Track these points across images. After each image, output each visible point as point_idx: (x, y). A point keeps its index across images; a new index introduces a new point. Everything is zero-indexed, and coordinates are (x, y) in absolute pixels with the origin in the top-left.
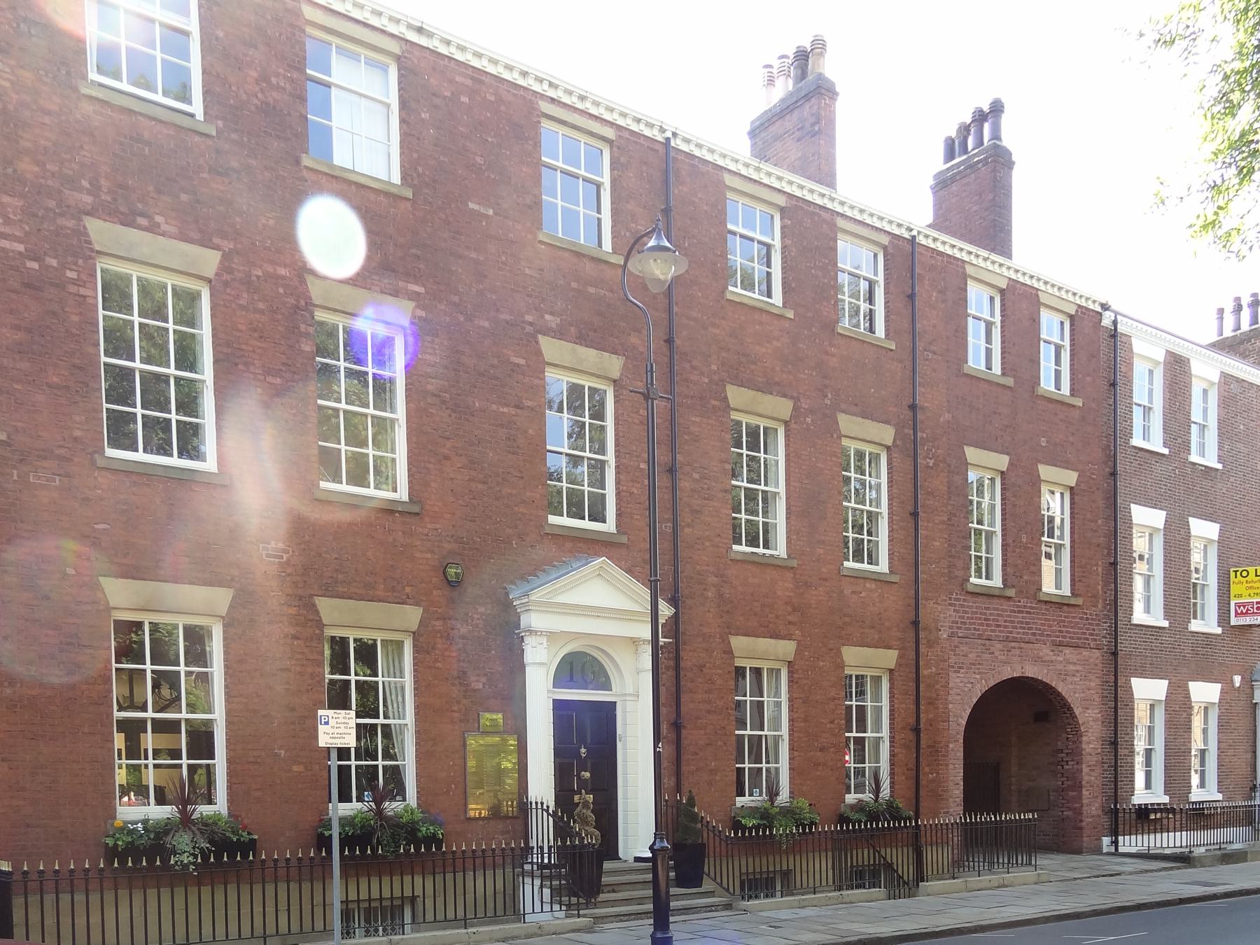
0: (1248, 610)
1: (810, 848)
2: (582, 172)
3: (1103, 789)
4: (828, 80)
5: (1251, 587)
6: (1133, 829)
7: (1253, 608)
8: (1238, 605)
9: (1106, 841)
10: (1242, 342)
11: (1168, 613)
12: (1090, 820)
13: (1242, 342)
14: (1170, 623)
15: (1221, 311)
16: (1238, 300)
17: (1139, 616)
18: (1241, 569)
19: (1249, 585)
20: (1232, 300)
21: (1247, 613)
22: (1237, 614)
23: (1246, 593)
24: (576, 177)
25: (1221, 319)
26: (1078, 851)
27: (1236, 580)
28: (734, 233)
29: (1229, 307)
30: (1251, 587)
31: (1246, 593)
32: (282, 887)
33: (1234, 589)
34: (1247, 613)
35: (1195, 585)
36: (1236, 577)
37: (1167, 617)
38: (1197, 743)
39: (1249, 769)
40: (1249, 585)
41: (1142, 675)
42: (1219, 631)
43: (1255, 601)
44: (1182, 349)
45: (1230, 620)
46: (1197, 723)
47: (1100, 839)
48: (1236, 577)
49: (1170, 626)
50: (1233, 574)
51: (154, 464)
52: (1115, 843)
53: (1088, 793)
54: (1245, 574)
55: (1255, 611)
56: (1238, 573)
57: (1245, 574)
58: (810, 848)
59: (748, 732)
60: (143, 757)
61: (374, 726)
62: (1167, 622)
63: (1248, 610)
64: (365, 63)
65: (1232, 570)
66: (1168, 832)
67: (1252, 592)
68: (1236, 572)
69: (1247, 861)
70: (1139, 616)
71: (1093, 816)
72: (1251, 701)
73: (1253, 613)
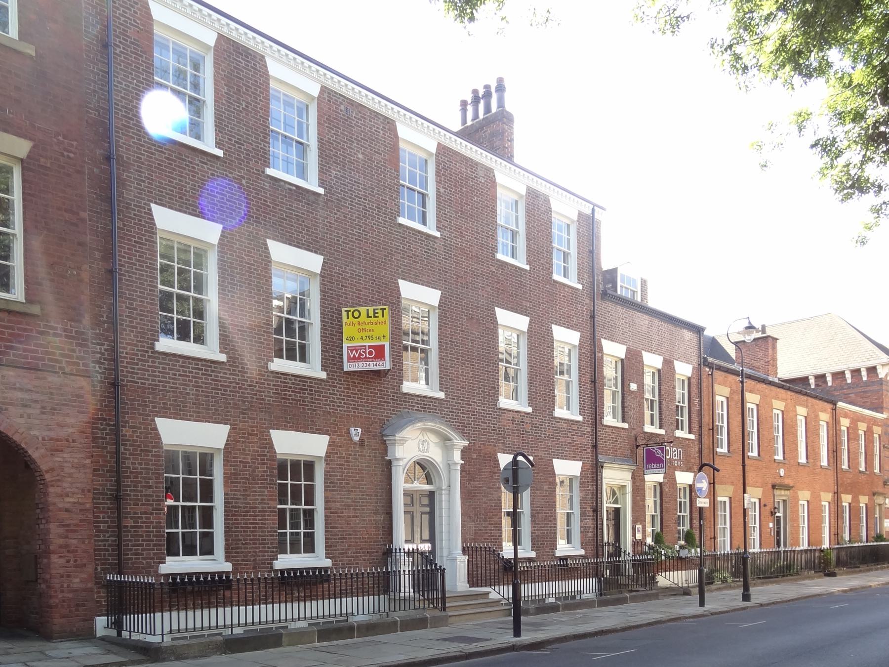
0: (360, 354)
1: (530, 581)
2: (418, 188)
3: (96, 555)
4: (507, 112)
5: (363, 330)
6: (276, 597)
7: (365, 352)
8: (351, 349)
9: (101, 623)
10: (477, 131)
11: (532, 400)
12: (70, 595)
13: (477, 131)
14: (327, 374)
15: (464, 104)
16: (475, 92)
17: (560, 412)
18: (352, 309)
19: (361, 327)
20: (470, 92)
21: (359, 358)
22: (350, 359)
23: (358, 335)
24: (414, 190)
25: (464, 110)
26: (48, 637)
27: (348, 321)
28: (403, 186)
29: (469, 98)
30: (363, 330)
31: (358, 335)
32: (544, 583)
33: (347, 331)
34: (359, 358)
35: (677, 406)
36: (348, 318)
37: (324, 367)
38: (561, 510)
39: (381, 532)
40: (361, 327)
41: (273, 429)
42: (323, 375)
43: (367, 344)
44: (542, 188)
45: (343, 366)
46: (561, 495)
47: (92, 620)
48: (348, 318)
49: (533, 412)
50: (344, 314)
51: (175, 355)
52: (118, 626)
53: (63, 561)
54: (356, 314)
55: (368, 356)
56: (350, 314)
57: (356, 314)
58: (530, 581)
59: (199, 504)
60: (173, 526)
61: (194, 507)
62: (325, 373)
63: (360, 354)
64: (280, 121)
65: (344, 310)
66: (266, 604)
67: (364, 334)
68: (348, 312)
69: (281, 646)
70: (560, 412)
71: (76, 591)
72: (383, 458)
73: (366, 358)
